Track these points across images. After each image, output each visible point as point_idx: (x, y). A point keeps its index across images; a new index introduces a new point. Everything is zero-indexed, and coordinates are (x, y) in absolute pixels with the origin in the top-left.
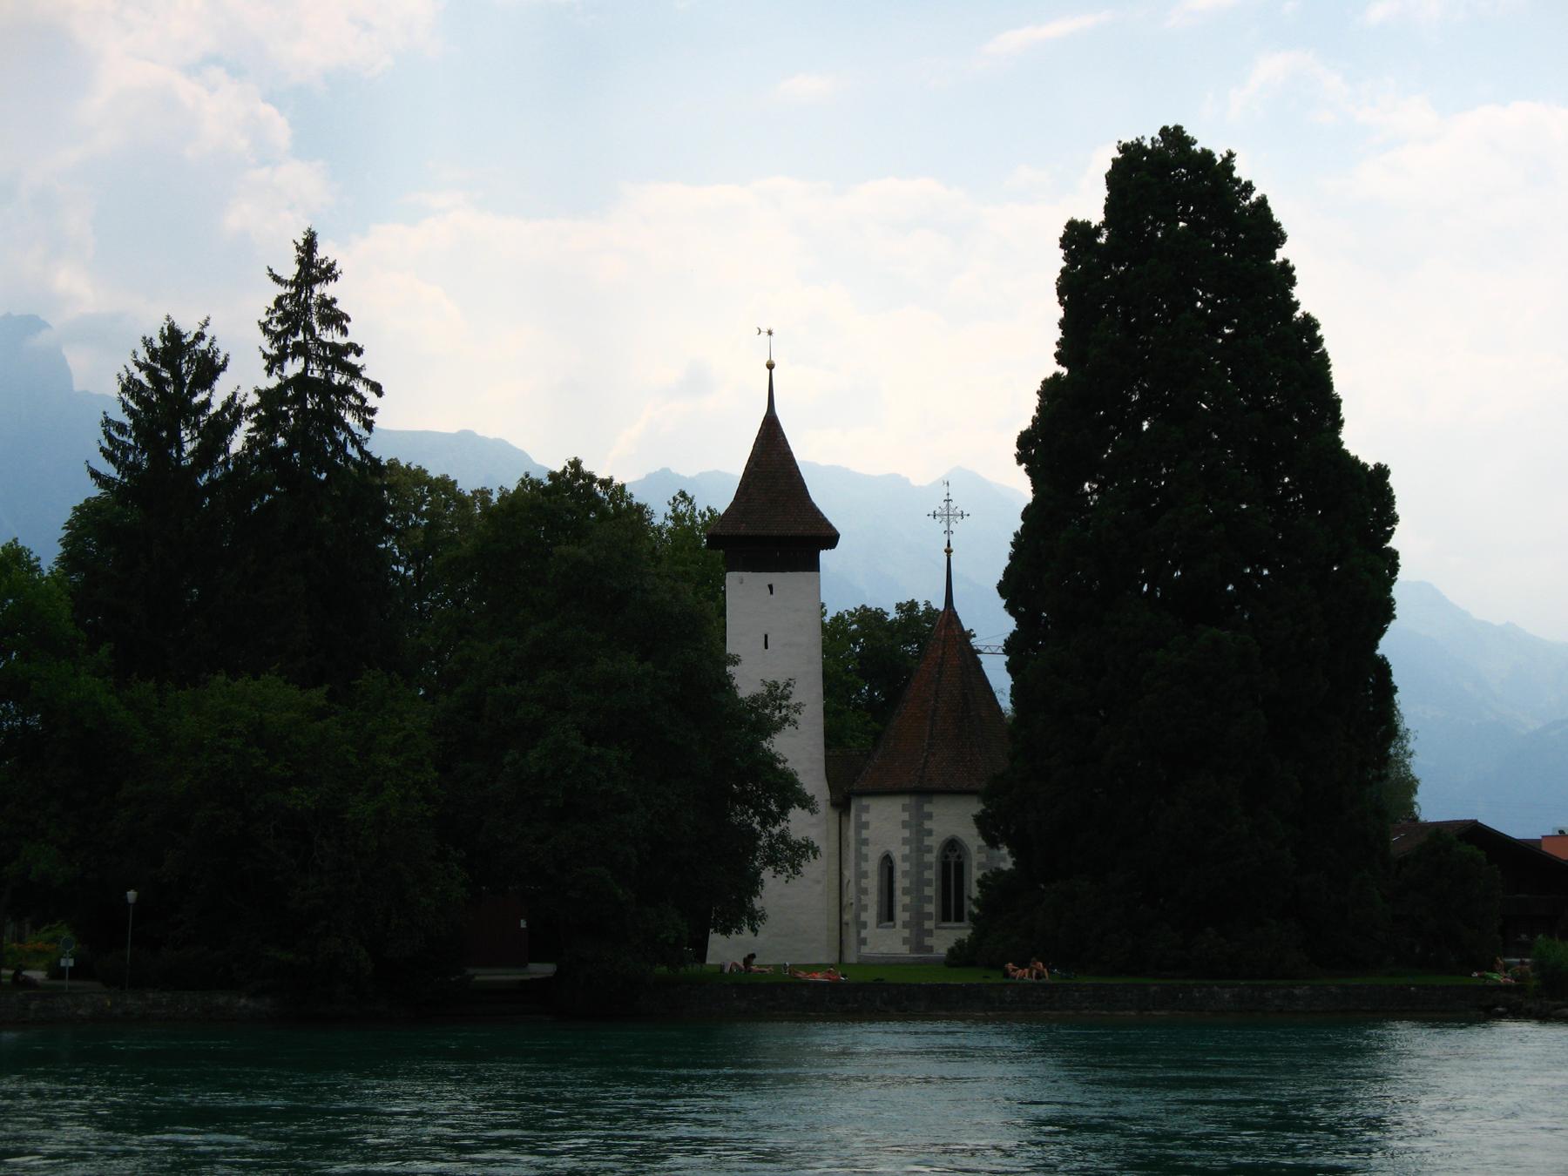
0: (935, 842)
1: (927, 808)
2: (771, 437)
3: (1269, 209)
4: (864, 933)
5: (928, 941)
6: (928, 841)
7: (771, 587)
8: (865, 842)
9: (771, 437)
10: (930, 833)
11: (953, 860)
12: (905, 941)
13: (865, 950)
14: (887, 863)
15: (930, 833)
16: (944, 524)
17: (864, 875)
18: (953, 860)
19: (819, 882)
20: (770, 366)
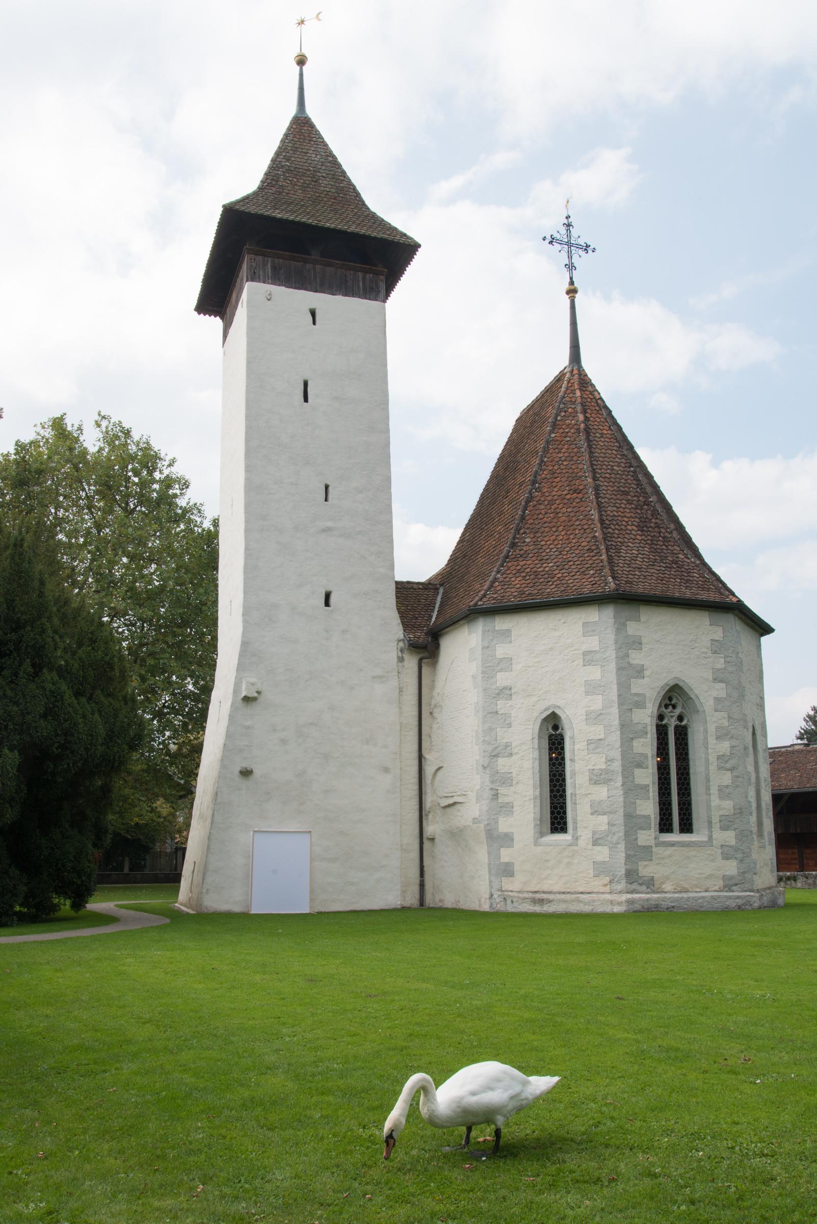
0: (650, 689)
1: (633, 628)
2: (302, 132)
3: (283, 141)
4: (506, 855)
5: (646, 870)
6: (638, 686)
7: (313, 313)
8: (506, 692)
9: (302, 132)
10: (640, 672)
11: (671, 723)
12: (600, 869)
13: (513, 885)
14: (117, 906)
15: (640, 672)
16: (564, 255)
17: (506, 751)
18: (671, 723)
19: (386, 770)
20: (301, 61)
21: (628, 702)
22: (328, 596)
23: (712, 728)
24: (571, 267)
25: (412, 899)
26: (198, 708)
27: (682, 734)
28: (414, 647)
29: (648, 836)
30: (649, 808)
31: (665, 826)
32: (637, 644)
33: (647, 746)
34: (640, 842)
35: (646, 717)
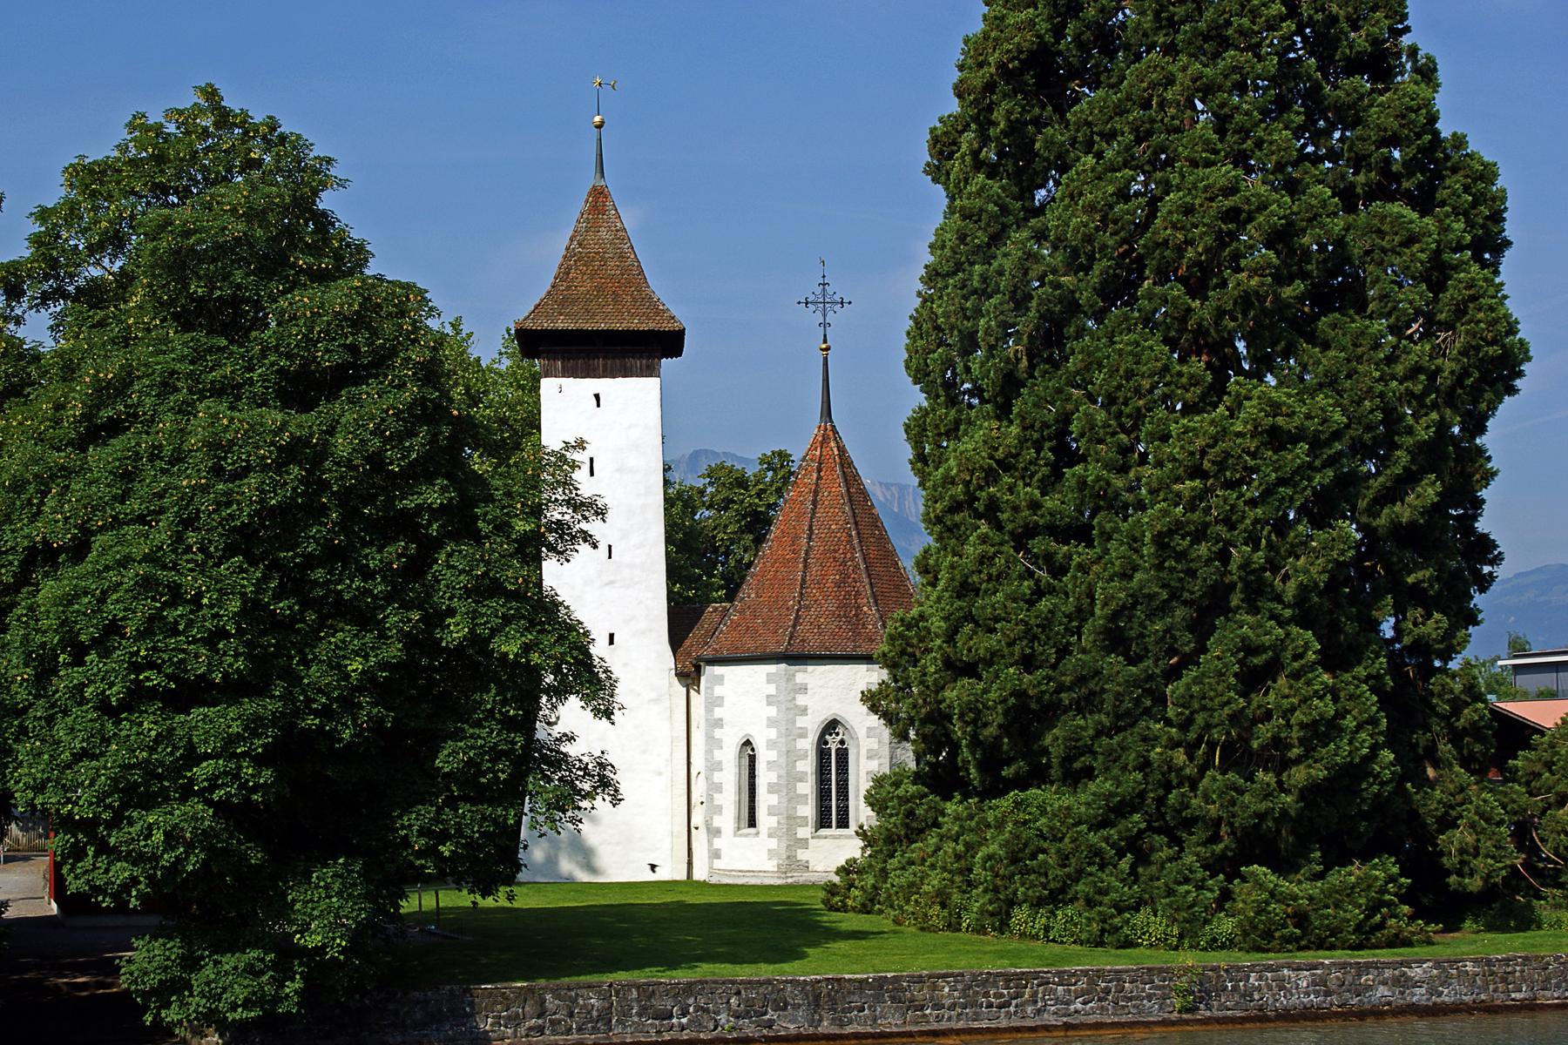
0: (812, 724)
6: (801, 722)
7: (597, 397)
8: (719, 723)
10: (804, 711)
11: (833, 747)
13: (718, 864)
15: (804, 711)
18: (833, 747)
19: (660, 774)
21: (793, 734)
22: (612, 636)
23: (863, 751)
24: (825, 325)
25: (682, 876)
26: (1326, 119)
27: (843, 756)
28: (681, 675)
29: (805, 832)
30: (808, 810)
31: (823, 821)
32: (803, 689)
33: (808, 766)
34: (799, 836)
35: (808, 744)
